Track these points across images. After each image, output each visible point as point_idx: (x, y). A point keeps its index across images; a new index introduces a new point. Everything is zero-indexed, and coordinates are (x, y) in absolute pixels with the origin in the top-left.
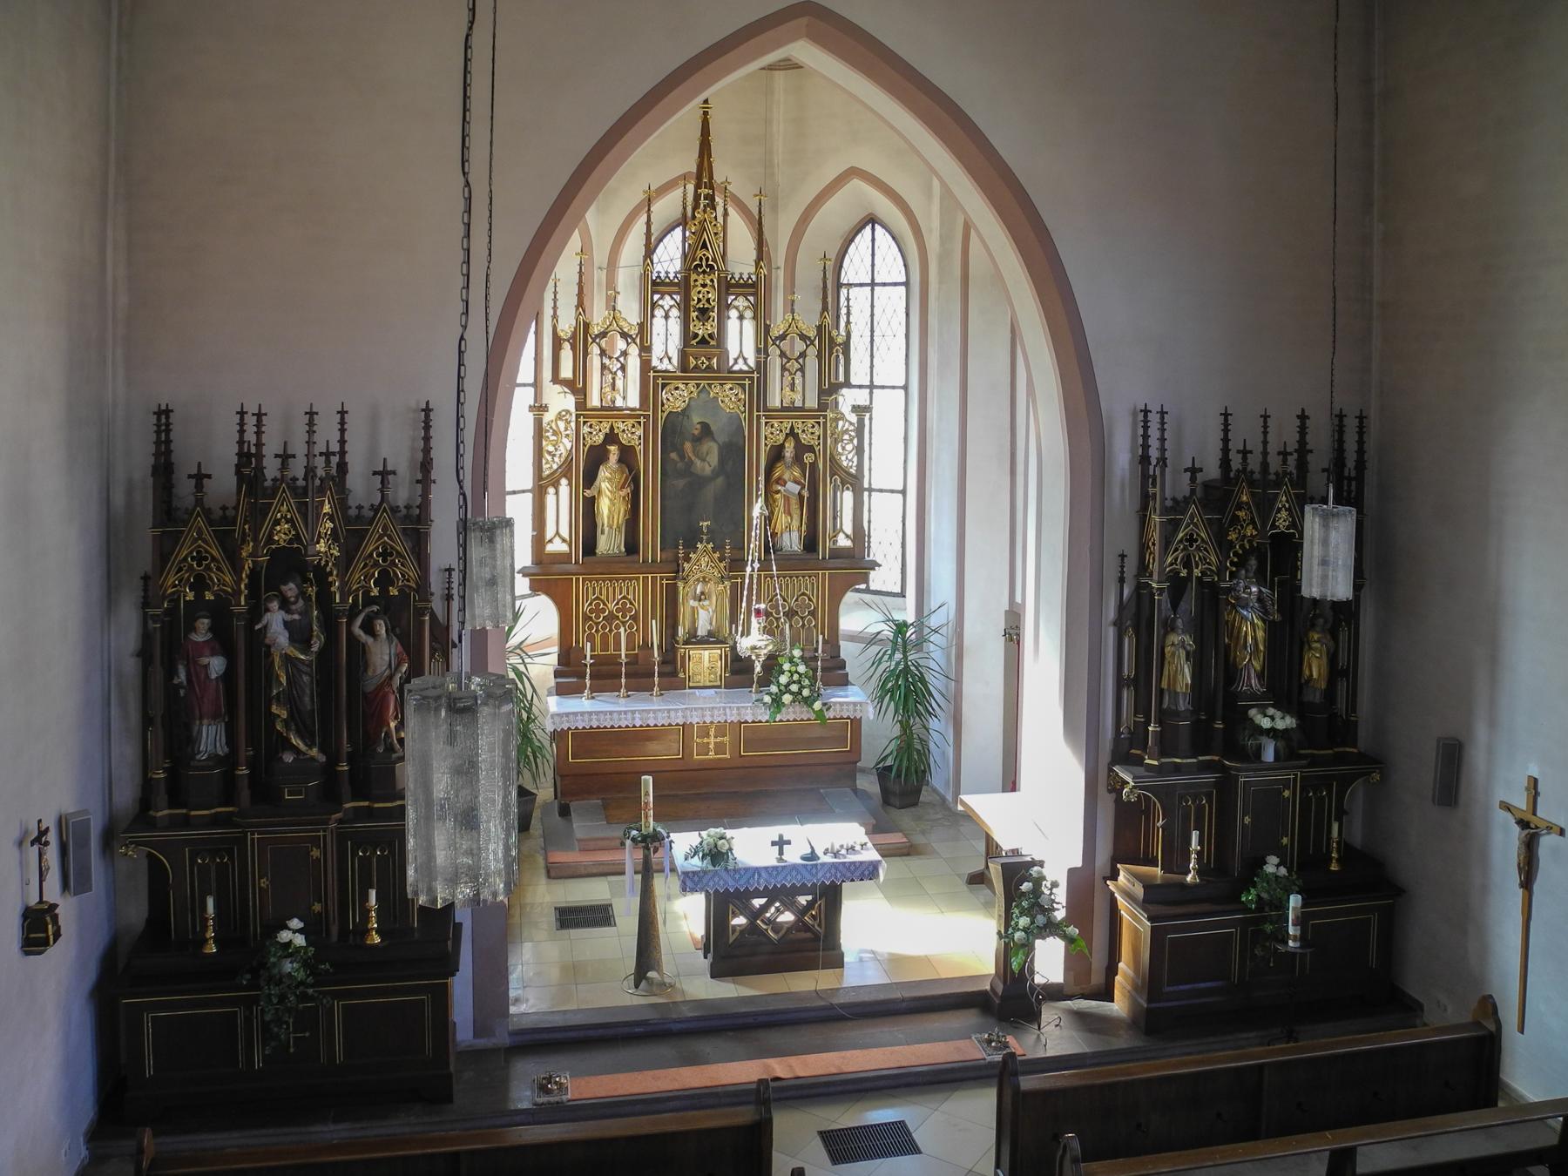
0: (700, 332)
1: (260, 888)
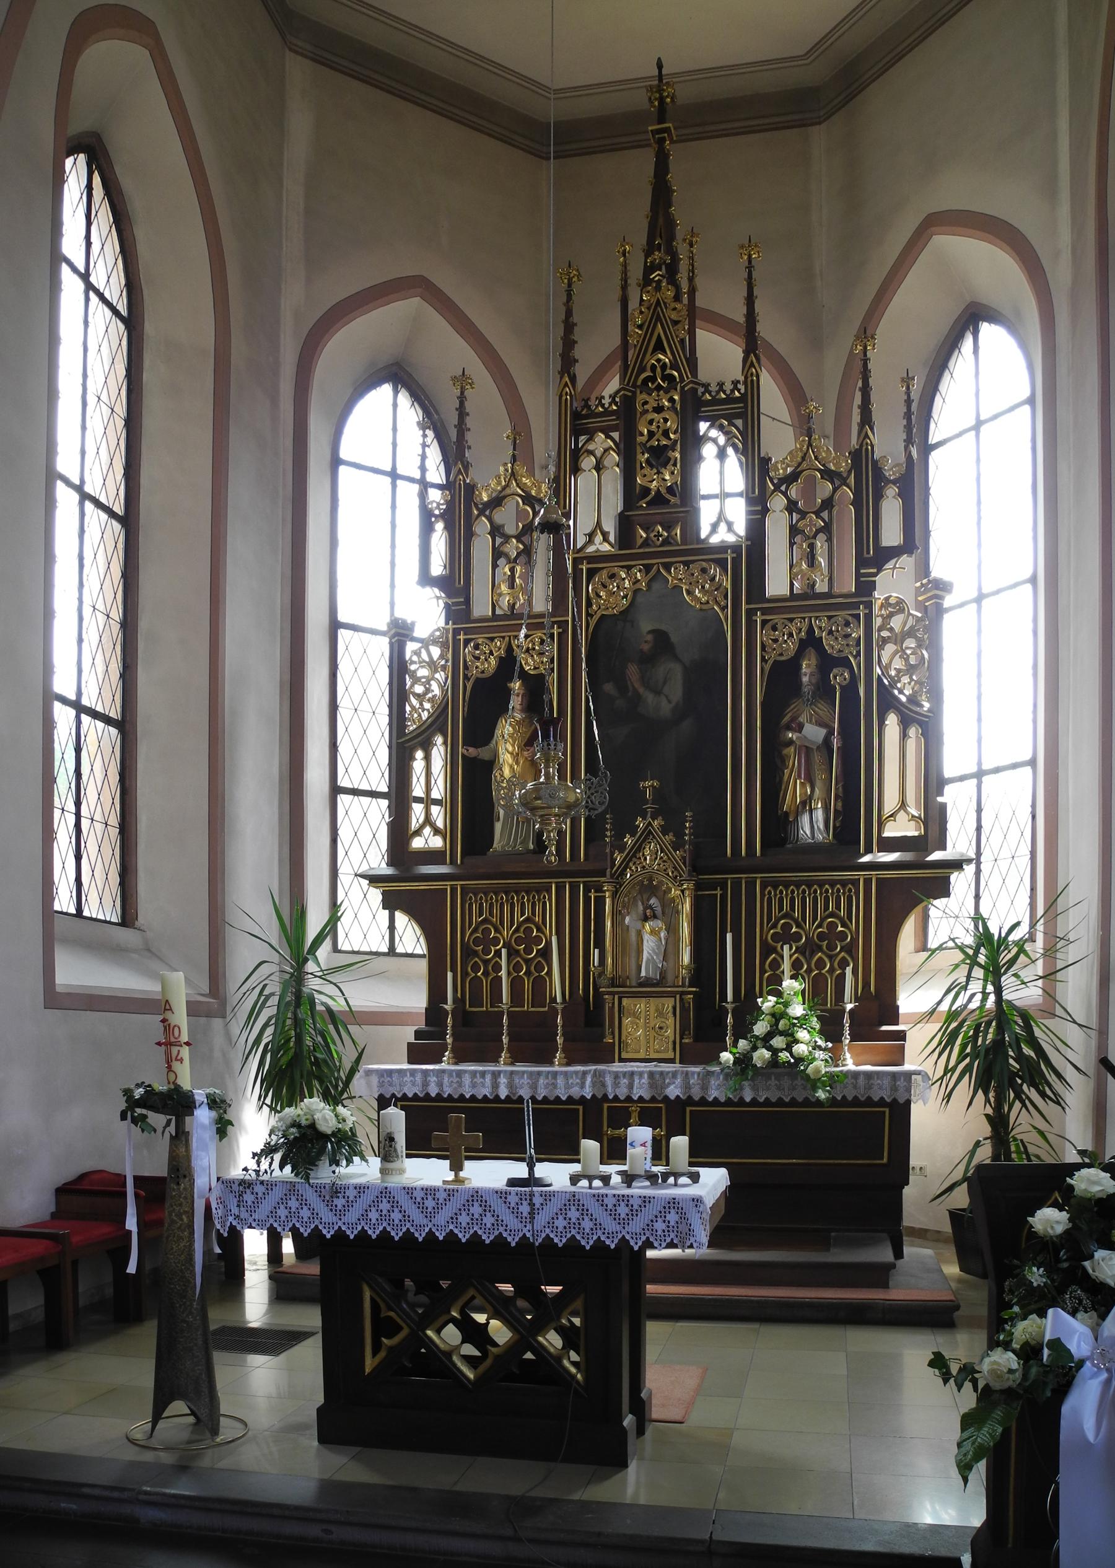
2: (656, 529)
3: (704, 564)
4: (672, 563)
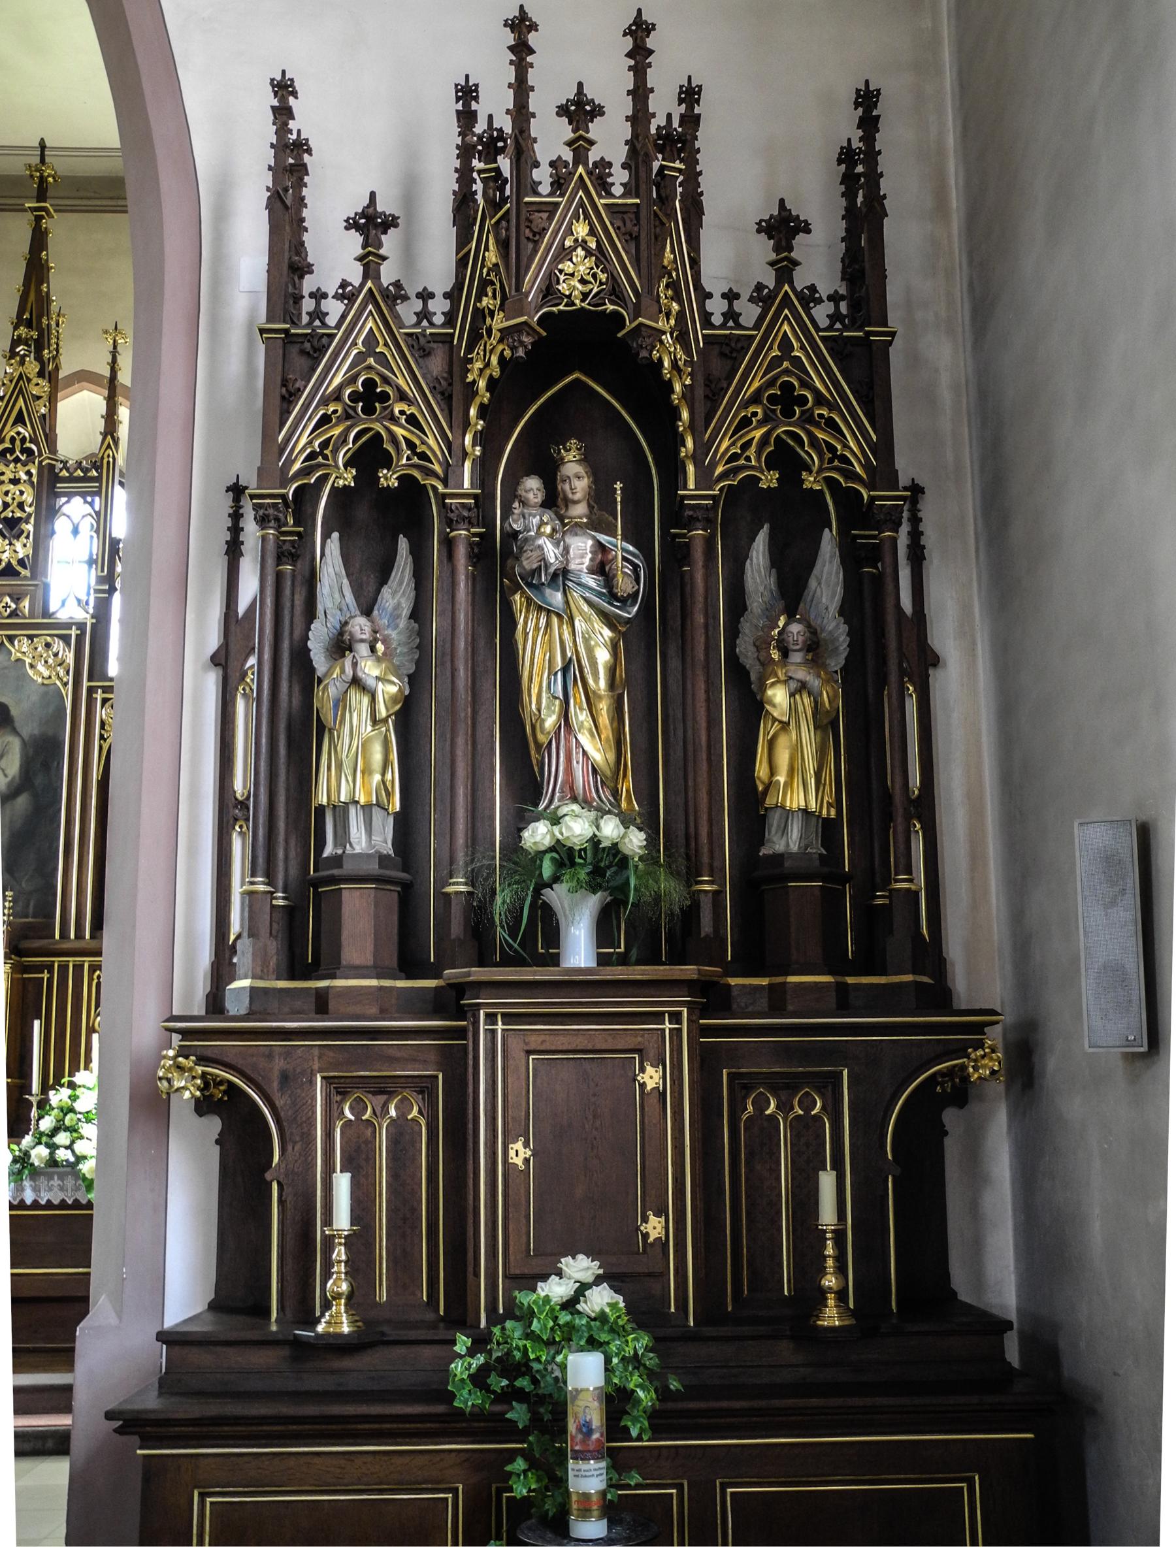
2: (4, 600)
3: (49, 639)
4: (16, 636)
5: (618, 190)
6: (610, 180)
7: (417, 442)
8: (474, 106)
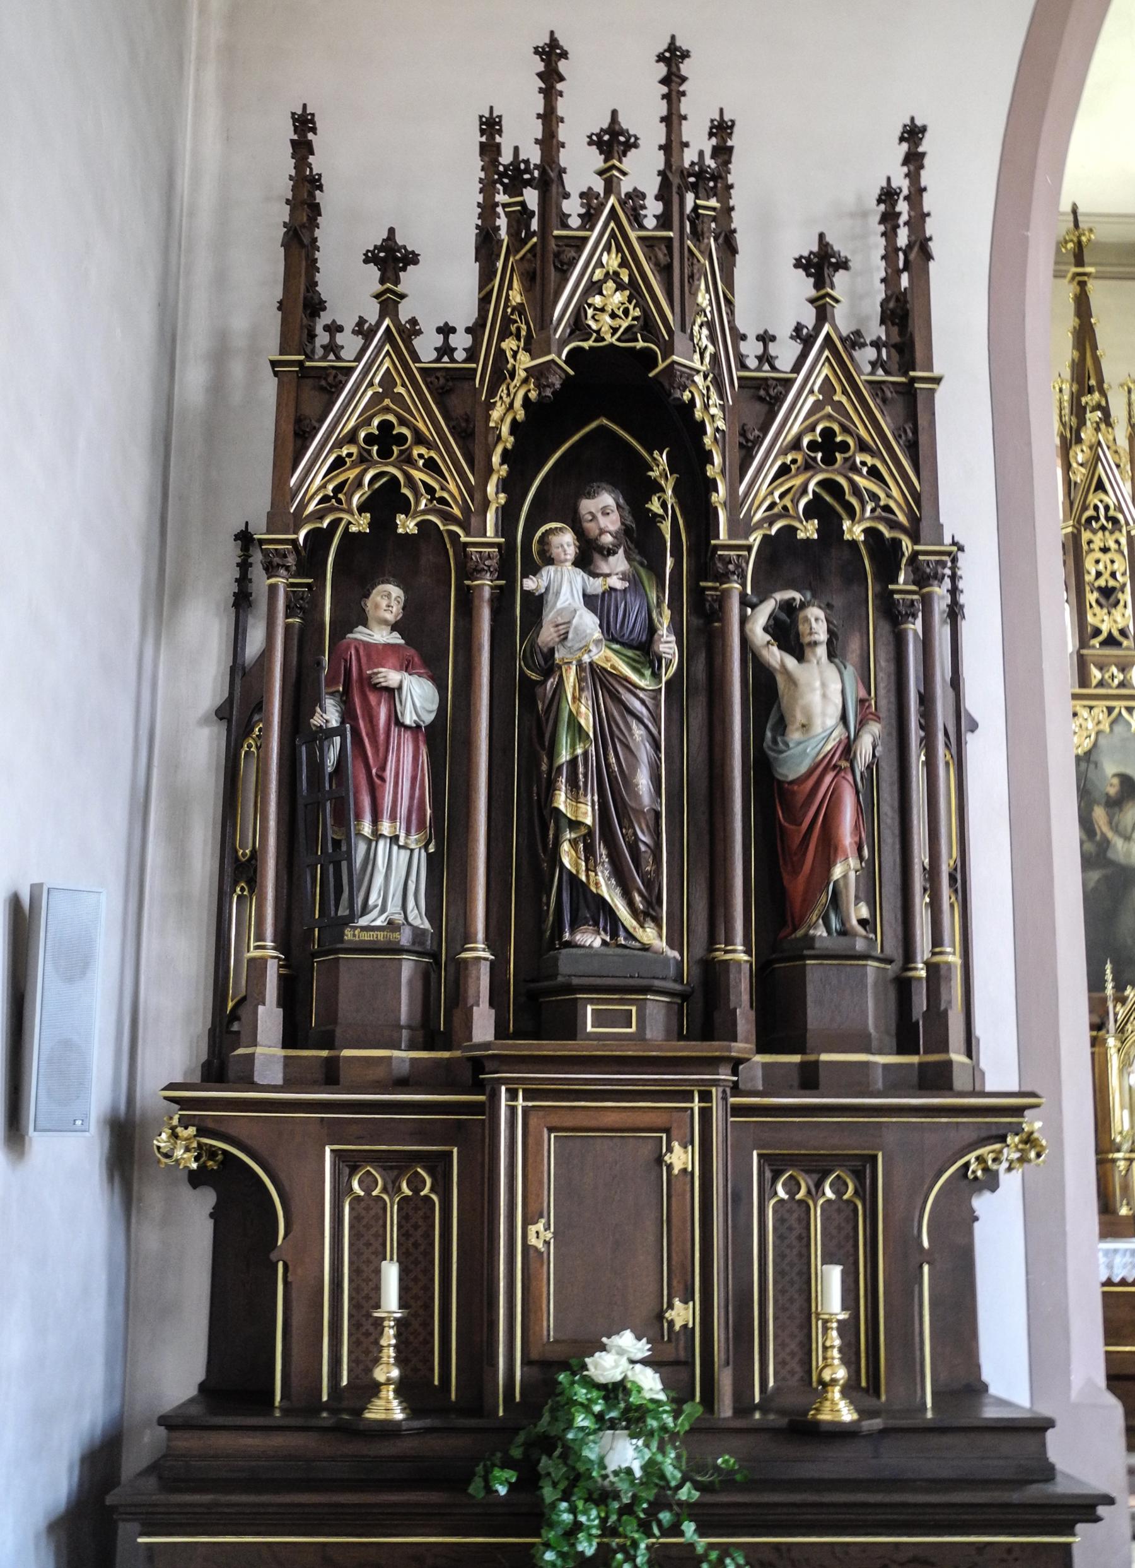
0: (1105, 628)
1: (526, 1247)
5: (650, 222)
6: (643, 212)
7: (437, 487)
8: (498, 139)
